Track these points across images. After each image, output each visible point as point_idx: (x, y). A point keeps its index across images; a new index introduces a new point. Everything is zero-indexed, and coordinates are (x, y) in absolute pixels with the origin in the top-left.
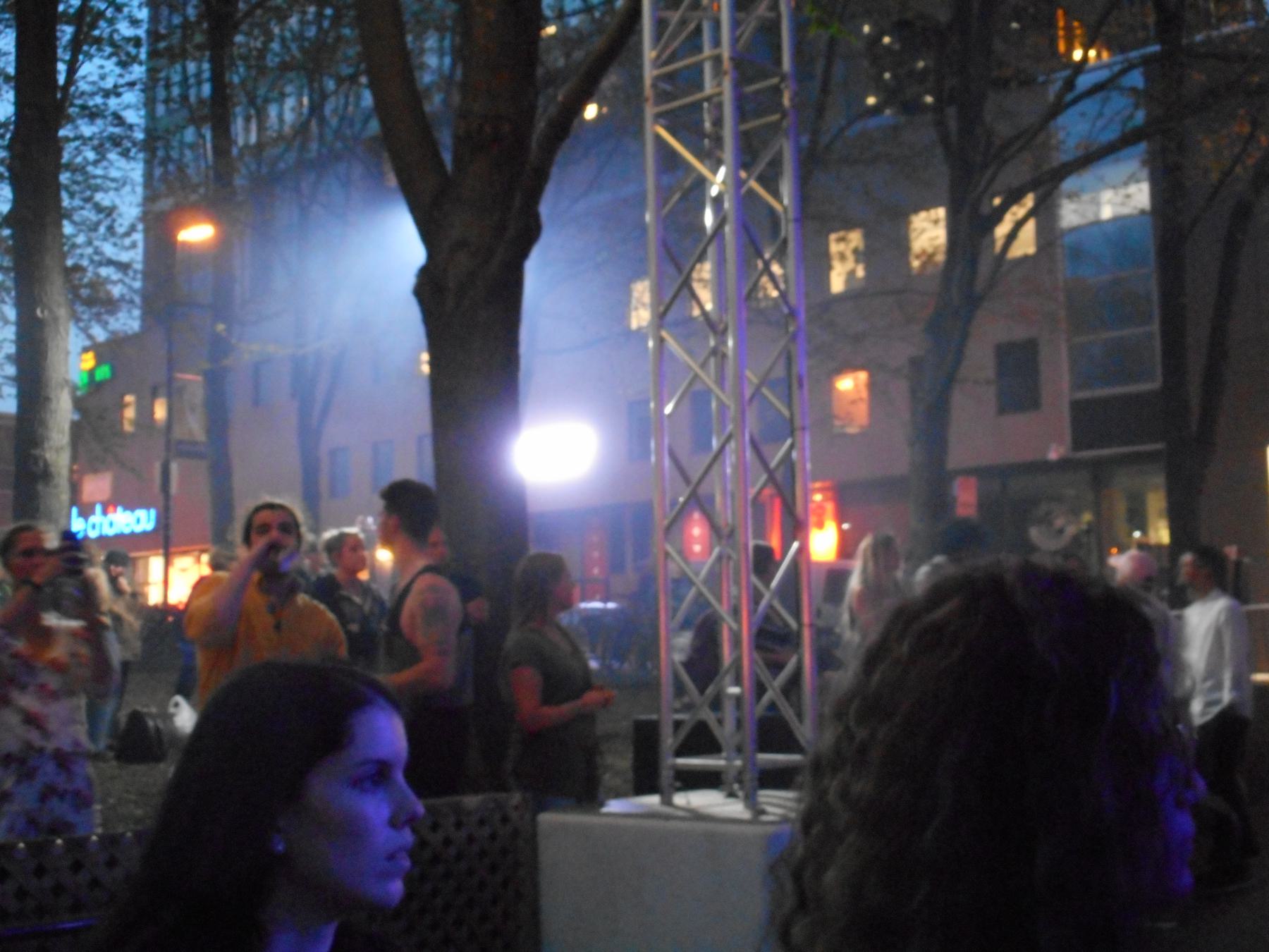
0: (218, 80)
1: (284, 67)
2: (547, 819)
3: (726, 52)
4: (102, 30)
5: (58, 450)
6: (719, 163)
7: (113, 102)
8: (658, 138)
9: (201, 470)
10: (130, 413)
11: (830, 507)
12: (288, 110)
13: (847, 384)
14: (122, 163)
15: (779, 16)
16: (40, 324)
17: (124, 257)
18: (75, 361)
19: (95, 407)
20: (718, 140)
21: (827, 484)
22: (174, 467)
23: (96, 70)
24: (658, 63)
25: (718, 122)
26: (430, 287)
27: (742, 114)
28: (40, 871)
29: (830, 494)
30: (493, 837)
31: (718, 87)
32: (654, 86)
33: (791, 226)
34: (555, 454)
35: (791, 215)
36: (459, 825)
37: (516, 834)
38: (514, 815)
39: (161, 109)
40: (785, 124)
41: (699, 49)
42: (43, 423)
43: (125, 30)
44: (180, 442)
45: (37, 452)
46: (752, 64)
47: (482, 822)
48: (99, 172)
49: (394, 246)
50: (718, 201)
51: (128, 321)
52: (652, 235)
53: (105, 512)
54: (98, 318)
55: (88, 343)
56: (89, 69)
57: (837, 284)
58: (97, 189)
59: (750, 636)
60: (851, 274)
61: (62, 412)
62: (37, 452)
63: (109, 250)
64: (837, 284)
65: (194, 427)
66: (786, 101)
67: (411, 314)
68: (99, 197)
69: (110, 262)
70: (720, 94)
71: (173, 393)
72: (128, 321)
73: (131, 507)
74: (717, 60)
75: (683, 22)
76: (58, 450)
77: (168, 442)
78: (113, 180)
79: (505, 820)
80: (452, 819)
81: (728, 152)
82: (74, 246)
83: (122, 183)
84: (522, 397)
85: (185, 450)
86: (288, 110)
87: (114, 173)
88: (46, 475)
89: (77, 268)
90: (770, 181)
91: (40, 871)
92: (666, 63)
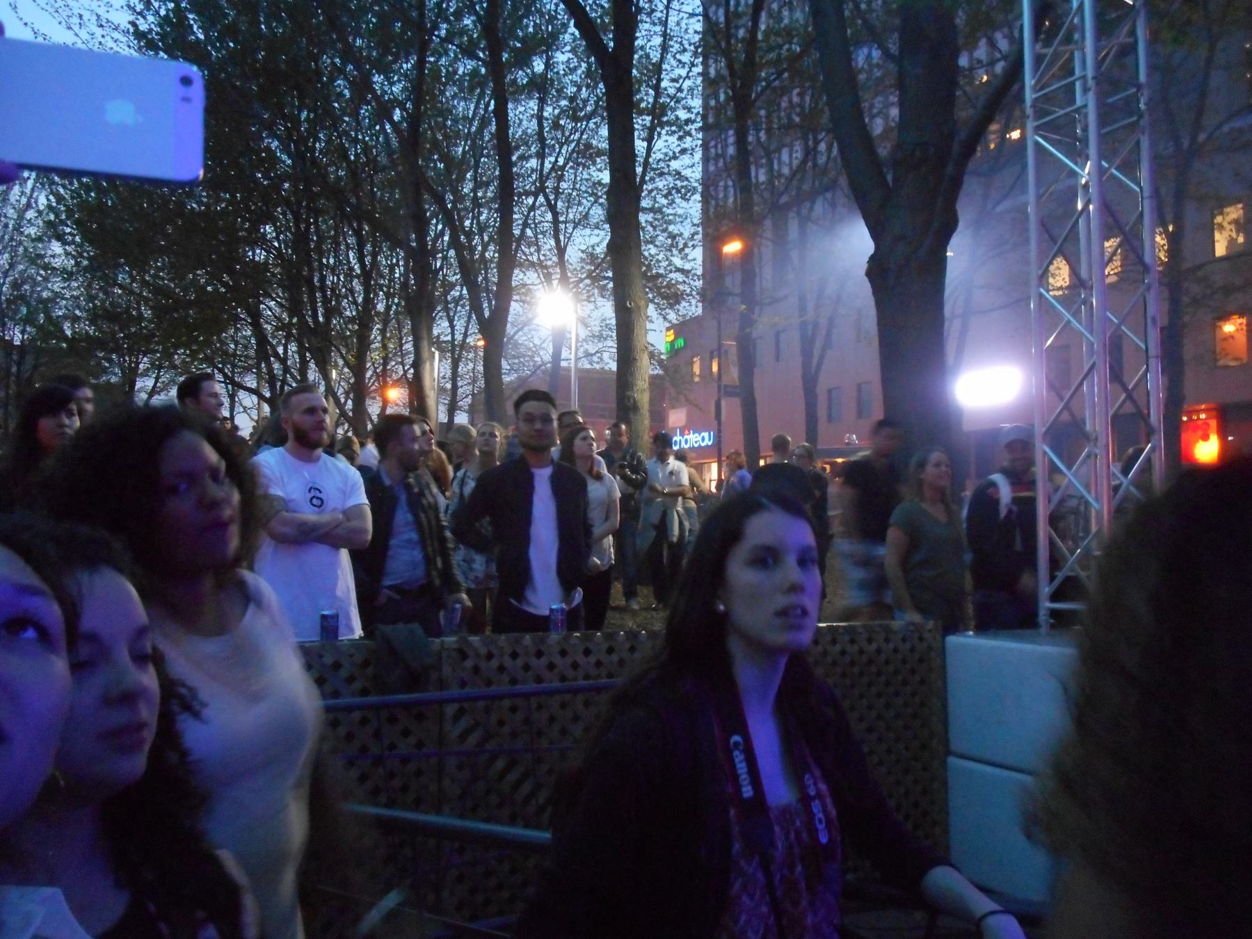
0: (741, 141)
1: (790, 126)
2: (953, 640)
3: (1090, 73)
4: (670, 116)
5: (643, 391)
6: (1087, 158)
7: (675, 165)
8: (1037, 144)
9: (736, 401)
10: (697, 369)
11: (1213, 423)
12: (789, 158)
13: (1229, 328)
14: (684, 204)
15: (1136, 42)
16: (629, 310)
17: (687, 266)
18: (657, 333)
19: (675, 363)
20: (1085, 141)
21: (1212, 405)
22: (723, 403)
23: (665, 142)
24: (1035, 89)
25: (1085, 129)
26: (877, 270)
27: (1103, 120)
28: (610, 650)
29: (1214, 413)
30: (912, 650)
31: (1087, 101)
32: (1033, 106)
33: (1147, 203)
34: (989, 386)
35: (1147, 193)
36: (887, 640)
37: (930, 648)
38: (927, 635)
39: (712, 168)
40: (1142, 122)
41: (1072, 73)
42: (632, 374)
43: (683, 115)
44: (726, 386)
45: (629, 393)
46: (1112, 78)
47: (904, 640)
48: (670, 211)
49: (856, 243)
50: (1086, 186)
51: (692, 308)
52: (1033, 219)
53: (682, 434)
54: (671, 306)
55: (668, 325)
56: (659, 144)
57: (1220, 249)
58: (670, 223)
59: (1109, 513)
60: (1232, 242)
61: (647, 369)
62: (629, 393)
63: (677, 262)
64: (1220, 249)
65: (734, 373)
66: (1142, 106)
67: (867, 287)
68: (671, 228)
69: (678, 270)
70: (1085, 106)
71: (719, 352)
72: (692, 308)
73: (698, 430)
74: (1084, 78)
75: (1056, 56)
76: (643, 391)
77: (719, 387)
78: (680, 216)
79: (921, 639)
80: (883, 636)
81: (1093, 150)
82: (658, 261)
83: (684, 217)
84: (951, 347)
85: (727, 391)
86: (789, 158)
87: (680, 211)
88: (635, 408)
89: (659, 276)
90: (1129, 167)
91: (610, 650)
92: (1042, 88)
